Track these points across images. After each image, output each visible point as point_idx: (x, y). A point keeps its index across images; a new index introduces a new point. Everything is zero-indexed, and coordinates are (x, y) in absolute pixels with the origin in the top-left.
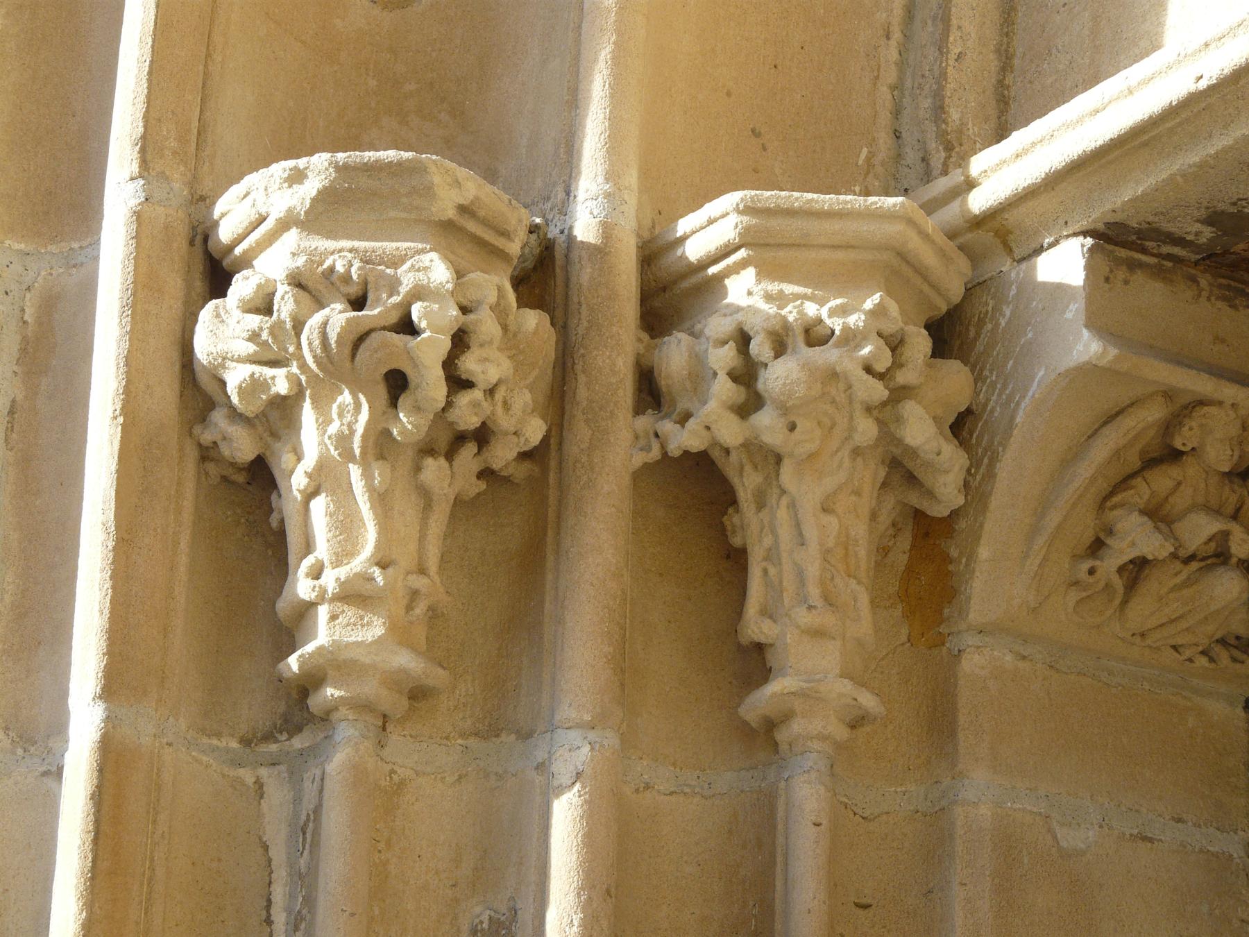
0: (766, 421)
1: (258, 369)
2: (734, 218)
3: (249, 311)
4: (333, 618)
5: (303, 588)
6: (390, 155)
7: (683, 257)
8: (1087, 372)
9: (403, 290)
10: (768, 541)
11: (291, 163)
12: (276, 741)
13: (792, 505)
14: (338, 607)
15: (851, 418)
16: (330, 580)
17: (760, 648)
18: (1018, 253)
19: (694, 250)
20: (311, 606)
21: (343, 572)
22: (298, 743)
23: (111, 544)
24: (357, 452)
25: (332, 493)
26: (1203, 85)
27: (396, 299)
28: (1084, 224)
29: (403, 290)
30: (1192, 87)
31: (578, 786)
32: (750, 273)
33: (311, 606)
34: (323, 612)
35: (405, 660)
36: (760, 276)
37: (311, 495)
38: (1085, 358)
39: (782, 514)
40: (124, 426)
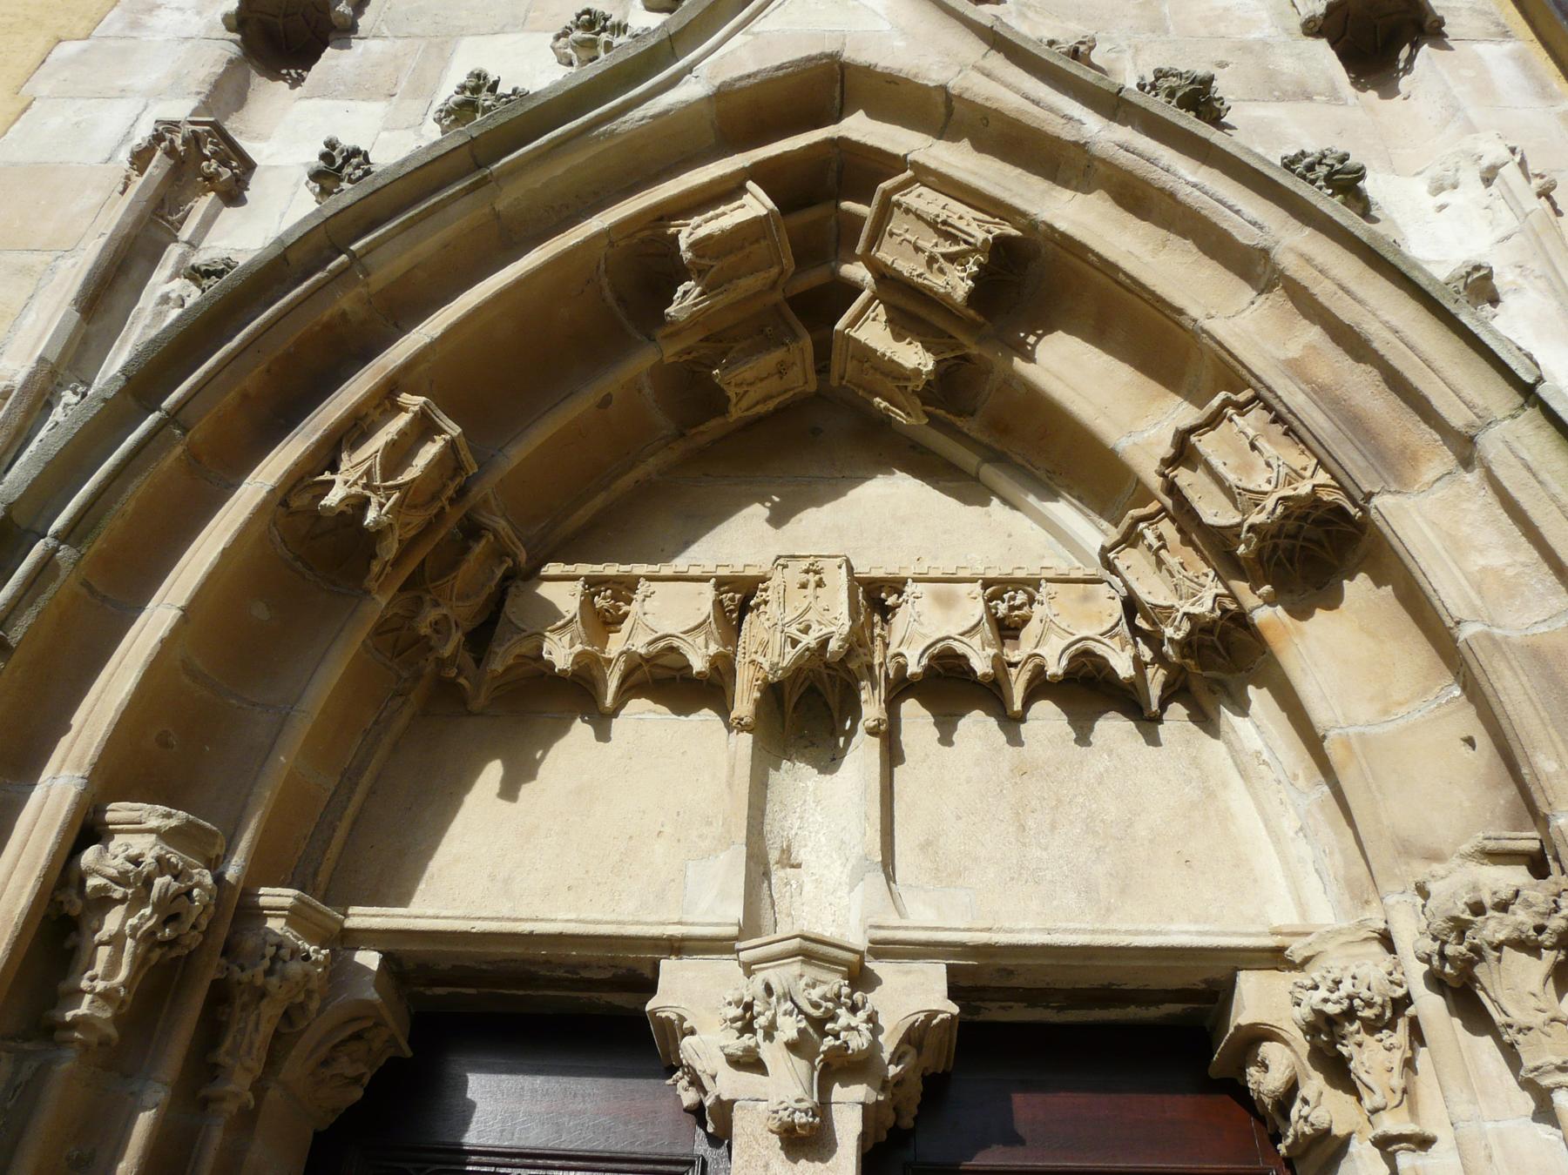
0: (274, 981)
1: (110, 883)
2: (291, 900)
3: (130, 862)
4: (92, 1002)
5: (84, 984)
6: (208, 825)
7: (257, 902)
8: (369, 1004)
9: (194, 881)
10: (242, 1025)
11: (168, 809)
12: (15, 1041)
13: (259, 1016)
14: (97, 998)
15: (299, 992)
16: (100, 985)
17: (216, 1065)
18: (345, 946)
19: (263, 901)
20: (83, 992)
21: (108, 984)
22: (26, 1046)
23: (16, 934)
24: (138, 936)
25: (114, 947)
26: (474, 930)
27: (190, 883)
28: (382, 948)
29: (194, 881)
30: (469, 929)
31: (154, 1111)
32: (282, 922)
33: (83, 992)
34: (88, 998)
35: (112, 1031)
36: (286, 924)
37: (102, 943)
38: (370, 998)
39: (253, 1017)
40: (43, 883)
